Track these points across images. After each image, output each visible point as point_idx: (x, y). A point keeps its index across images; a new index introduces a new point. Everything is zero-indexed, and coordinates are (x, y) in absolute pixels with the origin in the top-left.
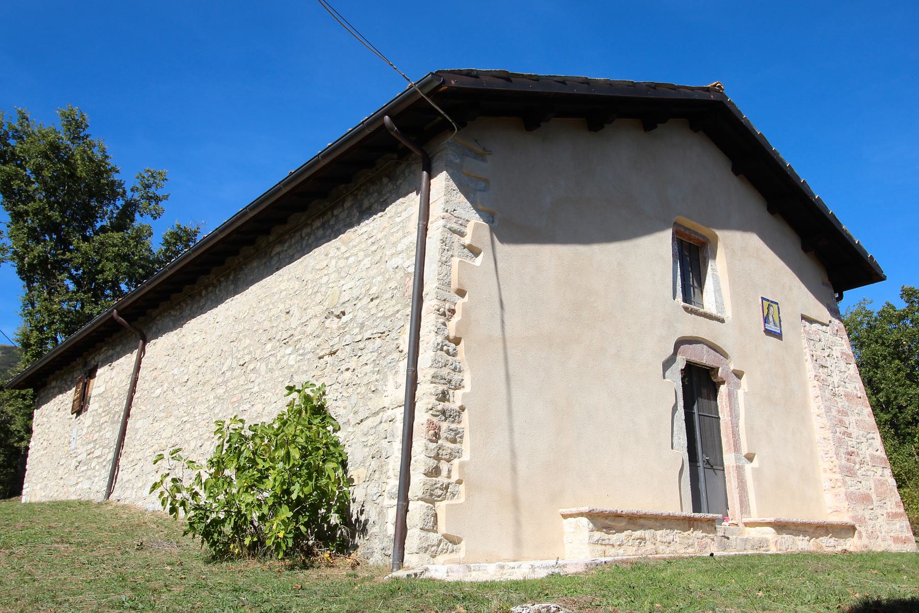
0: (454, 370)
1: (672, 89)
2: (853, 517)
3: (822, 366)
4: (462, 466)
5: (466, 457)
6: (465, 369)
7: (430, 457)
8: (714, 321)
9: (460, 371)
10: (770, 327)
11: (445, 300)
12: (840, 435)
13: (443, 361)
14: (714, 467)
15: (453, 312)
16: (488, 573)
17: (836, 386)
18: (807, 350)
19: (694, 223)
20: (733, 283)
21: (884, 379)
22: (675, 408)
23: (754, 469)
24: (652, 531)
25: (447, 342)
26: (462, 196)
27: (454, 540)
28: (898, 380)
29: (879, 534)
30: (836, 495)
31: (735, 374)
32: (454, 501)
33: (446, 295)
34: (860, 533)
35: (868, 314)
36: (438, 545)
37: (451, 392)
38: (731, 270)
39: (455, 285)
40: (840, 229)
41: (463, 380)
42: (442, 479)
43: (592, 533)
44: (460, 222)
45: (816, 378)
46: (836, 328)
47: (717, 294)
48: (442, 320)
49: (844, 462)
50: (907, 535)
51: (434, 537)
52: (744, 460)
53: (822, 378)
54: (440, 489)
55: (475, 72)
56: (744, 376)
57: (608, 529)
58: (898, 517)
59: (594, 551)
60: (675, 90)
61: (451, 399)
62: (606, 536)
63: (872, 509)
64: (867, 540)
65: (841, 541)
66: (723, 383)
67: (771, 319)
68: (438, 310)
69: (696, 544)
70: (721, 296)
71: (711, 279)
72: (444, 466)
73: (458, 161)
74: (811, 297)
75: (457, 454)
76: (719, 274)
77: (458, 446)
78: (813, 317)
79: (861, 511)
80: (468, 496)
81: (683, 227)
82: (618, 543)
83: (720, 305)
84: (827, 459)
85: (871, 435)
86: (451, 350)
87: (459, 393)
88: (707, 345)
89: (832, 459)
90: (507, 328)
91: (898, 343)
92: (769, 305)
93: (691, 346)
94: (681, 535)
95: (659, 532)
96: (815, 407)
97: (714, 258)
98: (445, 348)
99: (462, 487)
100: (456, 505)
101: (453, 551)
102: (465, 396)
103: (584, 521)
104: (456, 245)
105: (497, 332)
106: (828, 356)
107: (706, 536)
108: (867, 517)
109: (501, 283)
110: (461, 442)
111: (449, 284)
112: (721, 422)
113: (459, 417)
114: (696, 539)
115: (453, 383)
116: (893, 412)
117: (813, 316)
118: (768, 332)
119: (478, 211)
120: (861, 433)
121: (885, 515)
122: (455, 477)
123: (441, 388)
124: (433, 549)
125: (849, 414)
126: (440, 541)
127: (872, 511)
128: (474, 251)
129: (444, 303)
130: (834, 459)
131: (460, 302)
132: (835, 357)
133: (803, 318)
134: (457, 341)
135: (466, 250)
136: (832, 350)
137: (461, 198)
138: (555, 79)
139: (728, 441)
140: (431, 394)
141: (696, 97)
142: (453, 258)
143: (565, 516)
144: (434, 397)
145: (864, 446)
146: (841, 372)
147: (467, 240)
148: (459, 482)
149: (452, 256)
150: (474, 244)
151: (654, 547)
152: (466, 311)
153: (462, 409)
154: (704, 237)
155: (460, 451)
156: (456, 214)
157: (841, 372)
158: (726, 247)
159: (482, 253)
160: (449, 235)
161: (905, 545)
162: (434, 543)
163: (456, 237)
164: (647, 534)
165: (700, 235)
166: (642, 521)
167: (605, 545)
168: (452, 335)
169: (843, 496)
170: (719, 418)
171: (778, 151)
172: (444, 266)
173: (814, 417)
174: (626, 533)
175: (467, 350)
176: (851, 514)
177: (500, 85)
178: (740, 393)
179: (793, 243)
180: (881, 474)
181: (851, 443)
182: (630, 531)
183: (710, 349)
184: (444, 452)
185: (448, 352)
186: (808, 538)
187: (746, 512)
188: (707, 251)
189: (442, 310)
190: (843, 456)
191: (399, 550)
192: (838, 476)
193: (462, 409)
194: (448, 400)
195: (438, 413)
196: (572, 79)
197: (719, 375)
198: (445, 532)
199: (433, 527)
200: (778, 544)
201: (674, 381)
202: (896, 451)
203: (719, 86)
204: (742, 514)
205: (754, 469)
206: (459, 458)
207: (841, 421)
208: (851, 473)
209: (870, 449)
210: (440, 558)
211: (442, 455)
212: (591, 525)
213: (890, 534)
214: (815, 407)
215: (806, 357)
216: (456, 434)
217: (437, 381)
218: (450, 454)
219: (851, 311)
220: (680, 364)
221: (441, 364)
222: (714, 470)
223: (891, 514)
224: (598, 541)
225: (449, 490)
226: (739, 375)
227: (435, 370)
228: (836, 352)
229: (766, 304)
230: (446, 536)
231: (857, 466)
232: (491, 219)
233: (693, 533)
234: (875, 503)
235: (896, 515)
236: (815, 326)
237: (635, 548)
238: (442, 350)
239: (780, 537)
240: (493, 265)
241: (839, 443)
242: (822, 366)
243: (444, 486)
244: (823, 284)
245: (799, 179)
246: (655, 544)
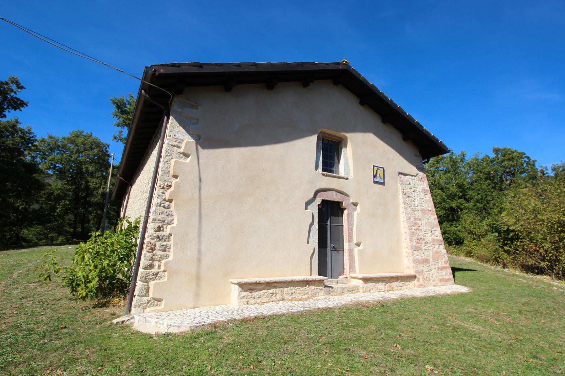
0: (168, 215)
1: (314, 65)
2: (415, 271)
3: (409, 197)
4: (166, 264)
5: (171, 258)
6: (175, 215)
7: (147, 260)
8: (342, 179)
9: (172, 216)
10: (378, 180)
11: (165, 181)
12: (414, 231)
13: (160, 211)
14: (338, 250)
15: (170, 186)
16: (151, 325)
17: (416, 206)
18: (400, 189)
19: (333, 132)
20: (355, 159)
21: (481, 189)
22: (312, 224)
23: (359, 251)
24: (281, 289)
25: (164, 202)
26: (181, 128)
27: (159, 300)
28: (489, 189)
29: (431, 278)
30: (409, 260)
31: (353, 204)
32: (161, 281)
33: (166, 178)
34: (419, 279)
35: (477, 160)
36: (148, 303)
37: (165, 227)
38: (354, 154)
39: (171, 173)
40: (422, 130)
41: (173, 220)
42: (155, 270)
43: (241, 293)
44: (178, 141)
45: (404, 203)
46: (421, 177)
47: (346, 166)
48: (162, 191)
49: (414, 244)
50: (449, 277)
51: (145, 299)
52: (354, 246)
53: (407, 203)
54: (152, 275)
55: (178, 65)
56: (359, 205)
57: (251, 290)
58: (445, 269)
59: (240, 302)
60: (316, 65)
61: (165, 230)
62: (250, 294)
63: (429, 266)
64: (422, 282)
65: (407, 283)
66: (346, 209)
67: (378, 175)
68: (160, 186)
69: (310, 293)
70: (348, 166)
71: (343, 158)
72: (156, 264)
73: (180, 110)
74: (406, 162)
75: (167, 256)
76: (348, 155)
77: (167, 253)
78: (406, 172)
79: (420, 267)
80: (169, 278)
81: (327, 134)
82: (258, 297)
83: (347, 171)
84: (405, 242)
85: (434, 229)
86: (166, 206)
87: (169, 227)
88: (336, 191)
89: (408, 243)
90: (202, 191)
91: (489, 173)
92: (378, 169)
93: (326, 193)
94: (300, 289)
95: (286, 289)
96: (402, 217)
97: (346, 146)
98: (162, 205)
99: (166, 273)
100: (161, 283)
101: (157, 305)
102: (172, 228)
103: (237, 286)
104: (175, 153)
105: (197, 195)
106: (414, 191)
107: (317, 288)
108: (425, 270)
109: (201, 170)
110: (169, 251)
111: (169, 173)
112: (344, 228)
113: (169, 238)
114: (310, 291)
115: (166, 222)
116: (484, 203)
117: (406, 172)
118: (375, 182)
119: (190, 134)
120: (428, 228)
121: (437, 268)
122: (162, 268)
123: (157, 225)
124: (144, 305)
125: (422, 219)
126: (149, 301)
127: (428, 267)
128: (187, 155)
129: (164, 182)
130: (409, 242)
131: (174, 181)
132: (418, 191)
133: (400, 173)
134: (170, 201)
135: (181, 155)
136: (417, 188)
137: (181, 129)
138: (233, 64)
139: (346, 237)
140: (151, 228)
141: (330, 68)
142: (172, 159)
143: (232, 283)
144: (153, 230)
145: (429, 235)
146: (420, 199)
147: (181, 150)
148: (165, 271)
149: (172, 158)
150: (185, 152)
151: (281, 297)
152: (177, 184)
153: (171, 234)
154: (340, 138)
155: (168, 255)
156: (176, 137)
157: (420, 199)
158: (352, 142)
159: (191, 156)
160: (171, 148)
161: (447, 282)
162: (145, 302)
163: (175, 149)
164: (278, 290)
165: (338, 137)
166: (275, 284)
167: (249, 298)
168: (167, 198)
169: (411, 261)
170: (343, 226)
171: (383, 92)
172: (166, 164)
173: (401, 222)
174: (263, 291)
175: (176, 206)
176: (414, 270)
177: (195, 70)
178: (355, 213)
179: (397, 137)
180: (437, 248)
181: (421, 234)
182: (266, 290)
183: (338, 193)
184: (157, 257)
185: (164, 207)
186: (384, 283)
187: (352, 271)
188: (342, 145)
189: (162, 186)
190: (415, 241)
191: (129, 305)
192: (410, 251)
193: (171, 234)
194: (163, 231)
195: (154, 238)
196: (245, 64)
197: (343, 205)
198: (152, 297)
199: (146, 294)
200: (364, 288)
201: (314, 209)
202: (480, 222)
203: (346, 62)
204: (350, 273)
205: (359, 251)
206: (166, 259)
207: (416, 224)
208: (418, 249)
209: (433, 236)
210: (148, 310)
211: (155, 258)
212: (240, 289)
213: (438, 278)
214: (402, 217)
215: (399, 193)
216: (165, 248)
217: (155, 222)
218: (160, 257)
219: (471, 158)
220: (318, 201)
221: (159, 213)
222: (337, 251)
223: (440, 268)
224: (244, 297)
225: (158, 275)
226: (355, 205)
227: (155, 216)
228: (419, 189)
229: (375, 169)
230: (153, 298)
231: (423, 245)
232: (199, 138)
233: (308, 287)
234: (431, 263)
235: (443, 268)
236: (407, 177)
237: (268, 298)
238: (160, 206)
239: (366, 285)
240: (197, 161)
241: (413, 234)
242: (409, 197)
243: (155, 274)
244: (416, 155)
245: (396, 106)
246: (282, 295)
